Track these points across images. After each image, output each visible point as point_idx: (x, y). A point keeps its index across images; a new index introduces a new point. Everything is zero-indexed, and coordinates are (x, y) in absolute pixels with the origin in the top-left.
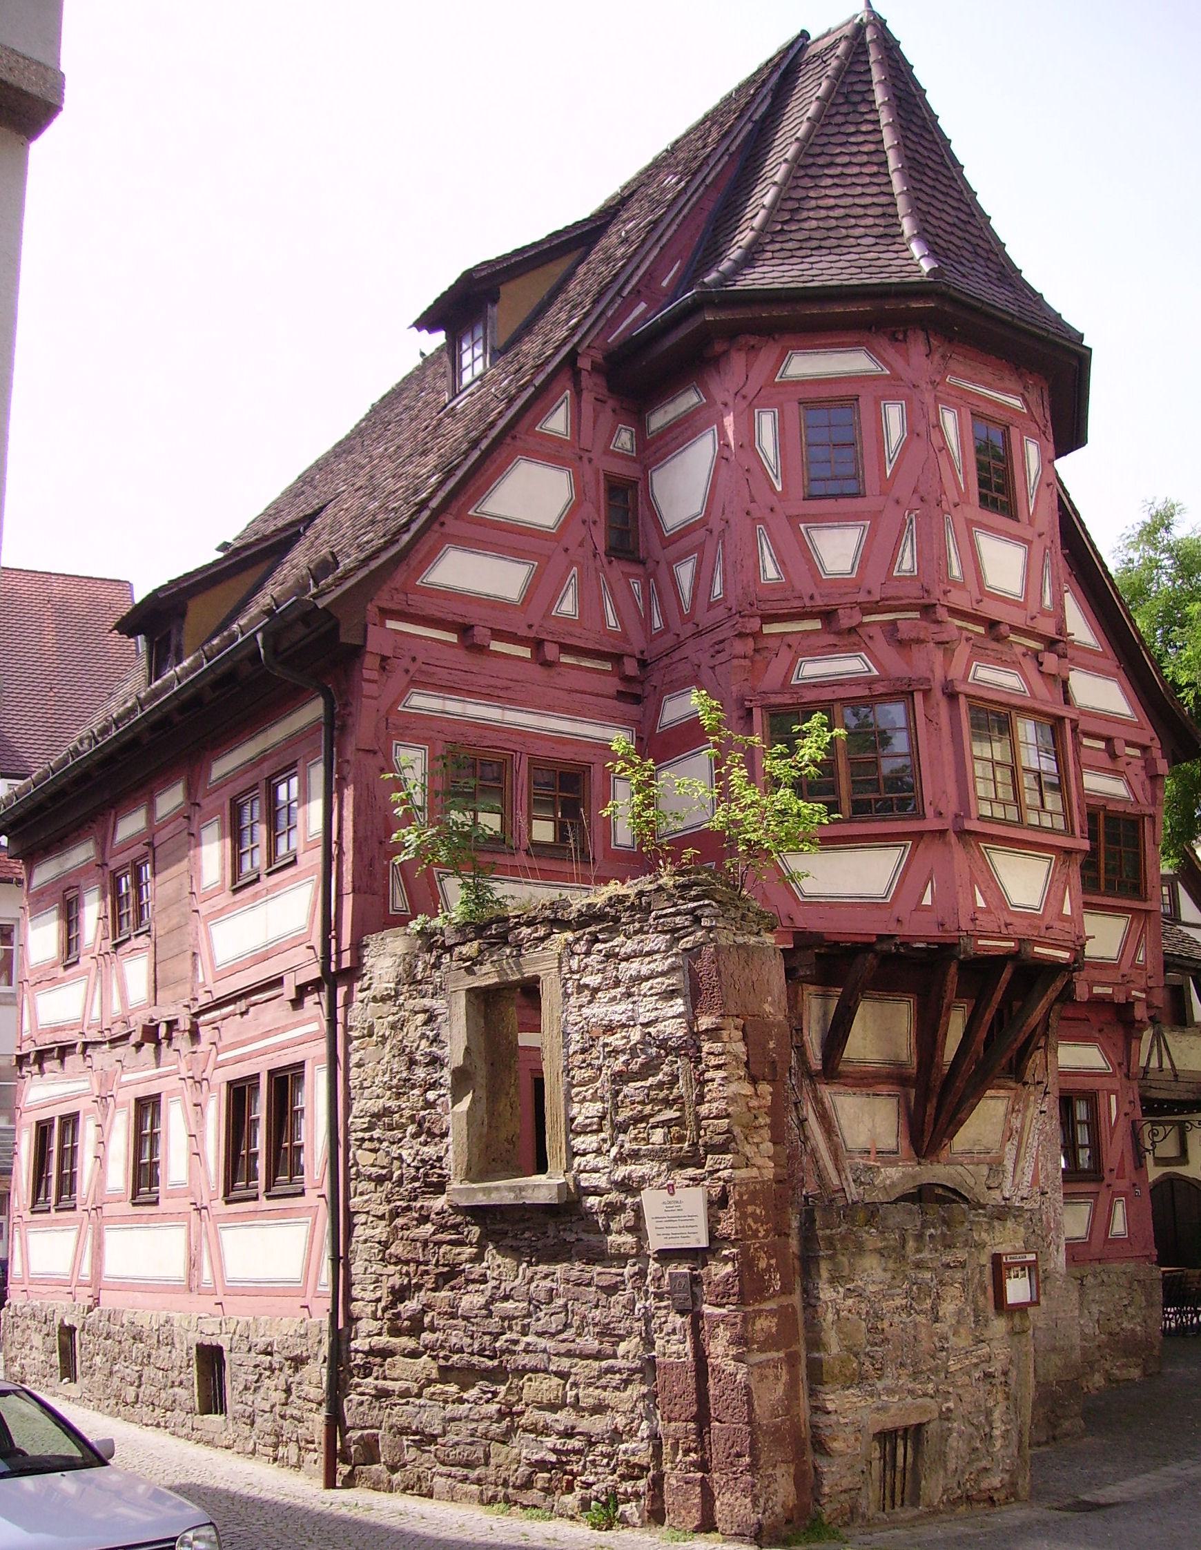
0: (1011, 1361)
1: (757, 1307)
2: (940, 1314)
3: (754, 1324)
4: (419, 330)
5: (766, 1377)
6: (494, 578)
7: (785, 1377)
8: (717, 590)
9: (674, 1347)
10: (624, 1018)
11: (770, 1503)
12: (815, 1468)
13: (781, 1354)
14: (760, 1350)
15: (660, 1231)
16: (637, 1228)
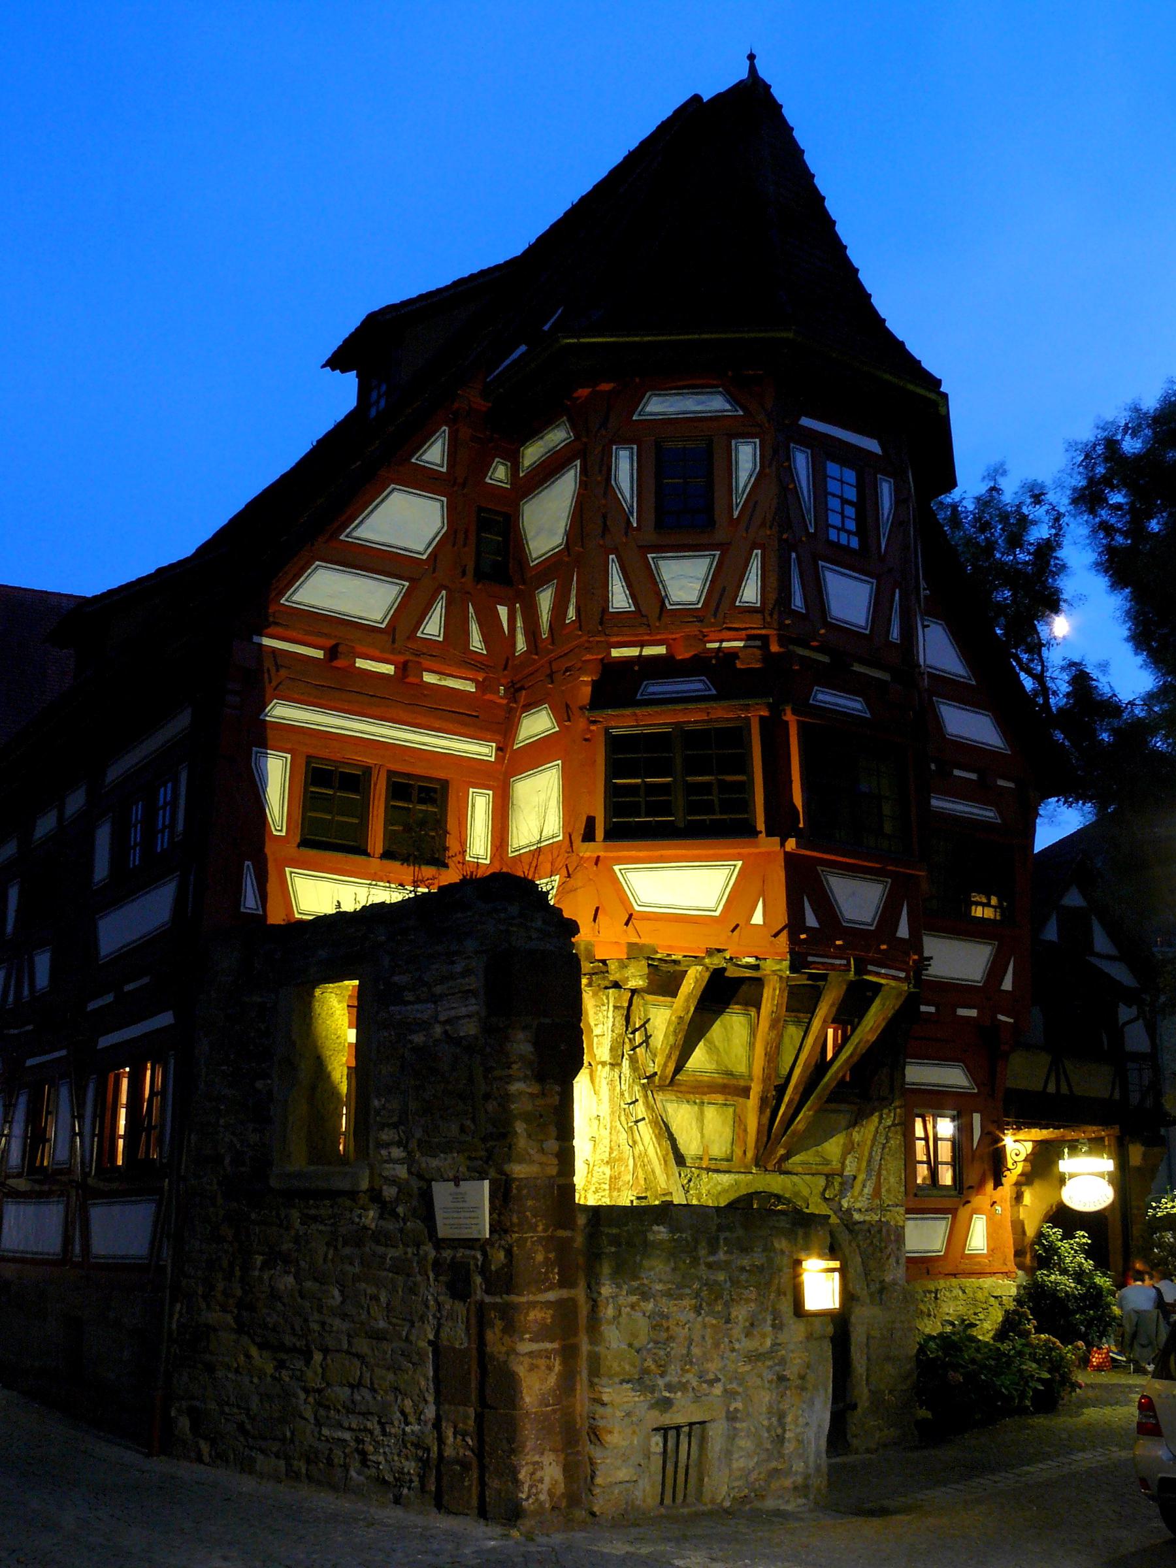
0: (808, 1366)
1: (531, 1298)
2: (733, 1316)
3: (527, 1314)
4: (333, 370)
5: (537, 1367)
6: (365, 599)
7: (557, 1368)
8: (571, 613)
9: (458, 1336)
10: (425, 1017)
11: (534, 1490)
12: (590, 1459)
13: (555, 1345)
14: (531, 1340)
15: (448, 1222)
16: (429, 1217)
